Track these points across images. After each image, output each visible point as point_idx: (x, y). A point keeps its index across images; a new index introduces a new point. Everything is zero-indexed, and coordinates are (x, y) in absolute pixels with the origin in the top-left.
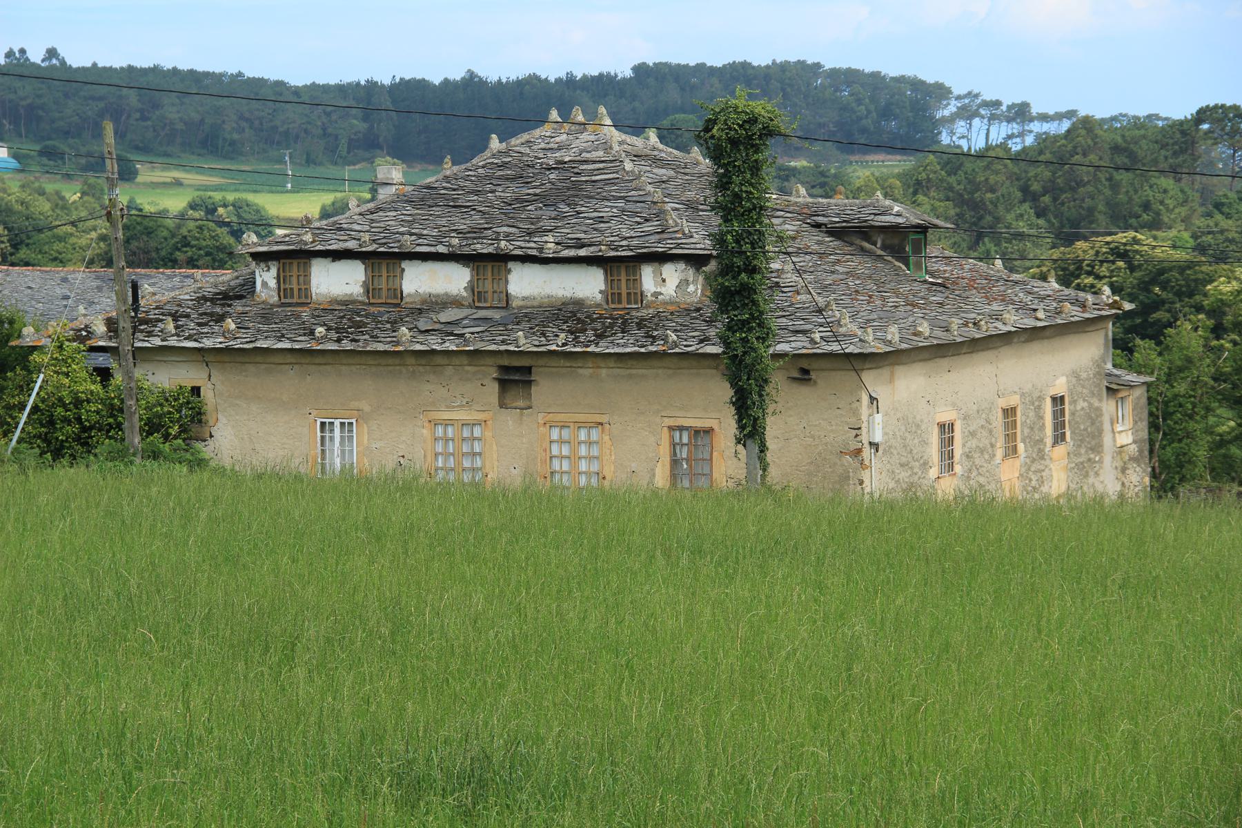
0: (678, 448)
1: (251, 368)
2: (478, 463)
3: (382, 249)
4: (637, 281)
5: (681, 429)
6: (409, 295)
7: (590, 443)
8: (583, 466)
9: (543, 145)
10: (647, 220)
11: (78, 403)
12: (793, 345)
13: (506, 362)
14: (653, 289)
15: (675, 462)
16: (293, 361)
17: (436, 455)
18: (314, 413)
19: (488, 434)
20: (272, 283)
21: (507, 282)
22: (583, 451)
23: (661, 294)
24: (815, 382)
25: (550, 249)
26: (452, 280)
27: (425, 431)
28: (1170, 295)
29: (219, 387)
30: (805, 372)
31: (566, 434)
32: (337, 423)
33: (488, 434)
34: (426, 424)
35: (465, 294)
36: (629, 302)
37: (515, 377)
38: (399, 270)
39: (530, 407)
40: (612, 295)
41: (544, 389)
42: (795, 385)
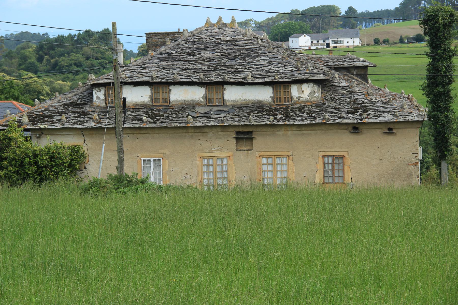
0: (326, 165)
1: (161, 135)
2: (225, 175)
3: (163, 81)
4: (289, 92)
5: (328, 156)
6: (174, 101)
7: (282, 164)
8: (219, 175)
9: (209, 34)
10: (285, 65)
11: (35, 156)
12: (387, 118)
13: (240, 130)
14: (297, 95)
15: (325, 171)
16: (130, 132)
17: (204, 172)
18: (140, 156)
19: (231, 162)
20: (102, 97)
21: (223, 94)
22: (279, 168)
23: (301, 97)
24: (396, 134)
25: (250, 79)
26: (197, 94)
27: (198, 162)
28: (375, 96)
29: (89, 145)
30: (390, 129)
31: (270, 161)
32: (152, 160)
33: (231, 162)
34: (199, 159)
35: (202, 100)
36: (285, 101)
37: (244, 136)
38: (168, 90)
39: (252, 150)
40: (276, 99)
41: (259, 142)
42: (350, 134)
